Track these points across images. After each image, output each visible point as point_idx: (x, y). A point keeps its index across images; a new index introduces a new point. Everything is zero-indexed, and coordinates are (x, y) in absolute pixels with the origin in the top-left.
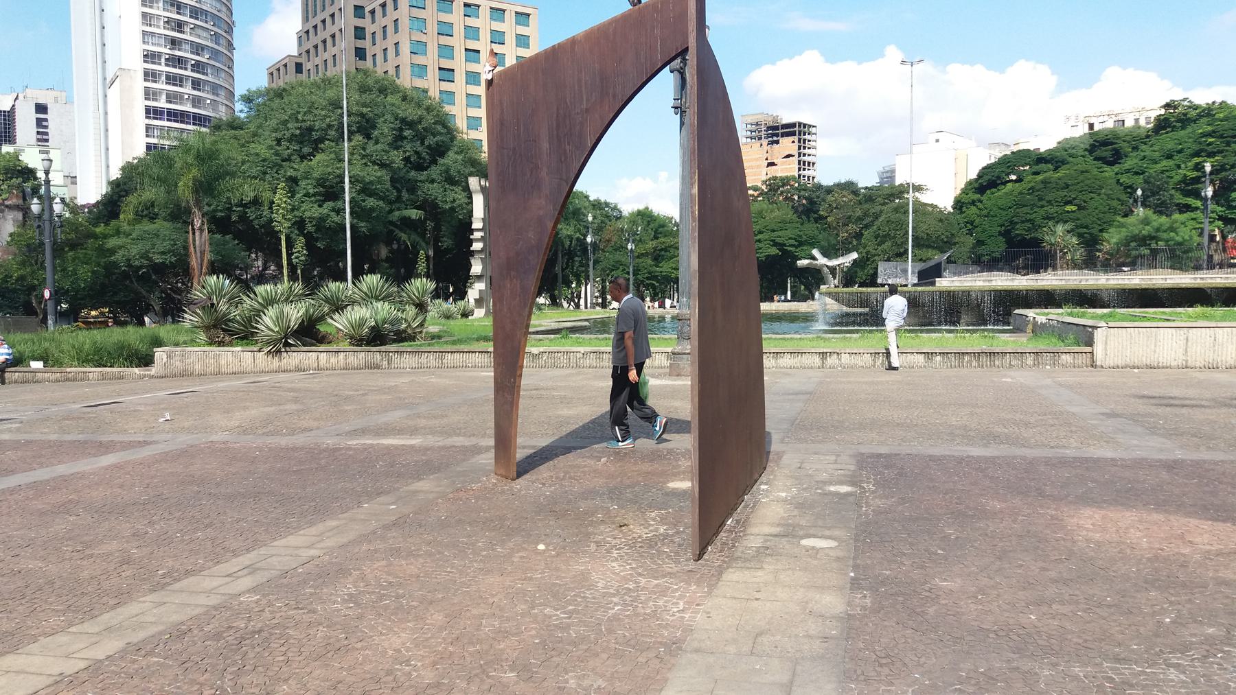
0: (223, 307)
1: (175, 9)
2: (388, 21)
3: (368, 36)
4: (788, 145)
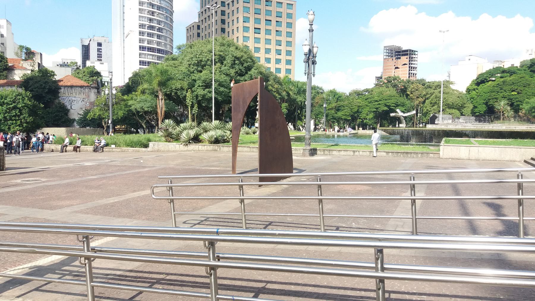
0: (170, 130)
1: (151, 7)
2: (234, 8)
3: (226, 14)
4: (404, 59)
